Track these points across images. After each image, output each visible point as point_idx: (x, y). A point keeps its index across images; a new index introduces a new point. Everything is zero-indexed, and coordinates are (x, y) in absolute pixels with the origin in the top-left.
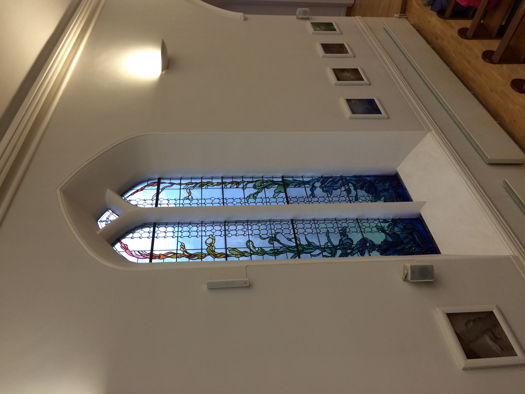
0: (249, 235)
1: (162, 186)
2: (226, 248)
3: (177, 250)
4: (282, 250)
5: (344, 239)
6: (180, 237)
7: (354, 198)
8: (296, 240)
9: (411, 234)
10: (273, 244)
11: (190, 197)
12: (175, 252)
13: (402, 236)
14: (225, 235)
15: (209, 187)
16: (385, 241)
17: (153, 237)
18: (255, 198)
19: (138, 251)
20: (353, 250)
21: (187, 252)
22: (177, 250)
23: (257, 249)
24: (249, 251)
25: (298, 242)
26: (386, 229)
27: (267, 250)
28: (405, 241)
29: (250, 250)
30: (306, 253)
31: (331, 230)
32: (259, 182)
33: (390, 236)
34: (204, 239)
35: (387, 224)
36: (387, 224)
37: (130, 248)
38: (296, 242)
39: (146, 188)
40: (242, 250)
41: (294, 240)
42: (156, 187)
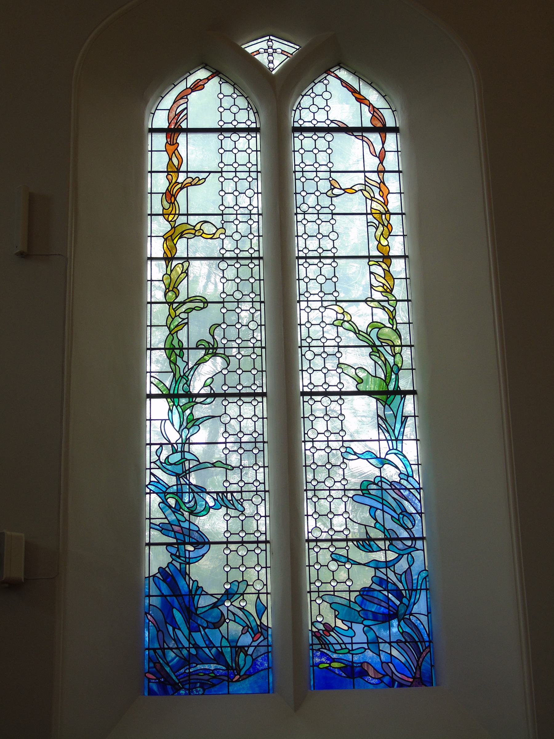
0: (226, 443)
1: (375, 137)
2: (188, 259)
3: (151, 372)
4: (181, 364)
5: (208, 499)
6: (226, 448)
7: (343, 552)
8: (207, 396)
9: (219, 658)
10: (197, 348)
11: (336, 191)
12: (183, 168)
13: (215, 636)
14: (223, 259)
15: (372, 230)
16: (199, 591)
17: (220, 130)
18: (338, 323)
19: (186, 108)
20: (176, 510)
21: (181, 189)
22: (187, 172)
23: (183, 316)
24: (180, 299)
25: (199, 400)
26: (236, 604)
27: (182, 335)
28: (197, 636)
29: (184, 303)
30: (170, 410)
31: (234, 477)
32: (394, 337)
33: (215, 606)
34: (216, 220)
35: (251, 608)
36: (251, 608)
37: (193, 97)
38: (199, 395)
39: (365, 108)
40: (182, 287)
41: (206, 390)
42: (367, 123)
